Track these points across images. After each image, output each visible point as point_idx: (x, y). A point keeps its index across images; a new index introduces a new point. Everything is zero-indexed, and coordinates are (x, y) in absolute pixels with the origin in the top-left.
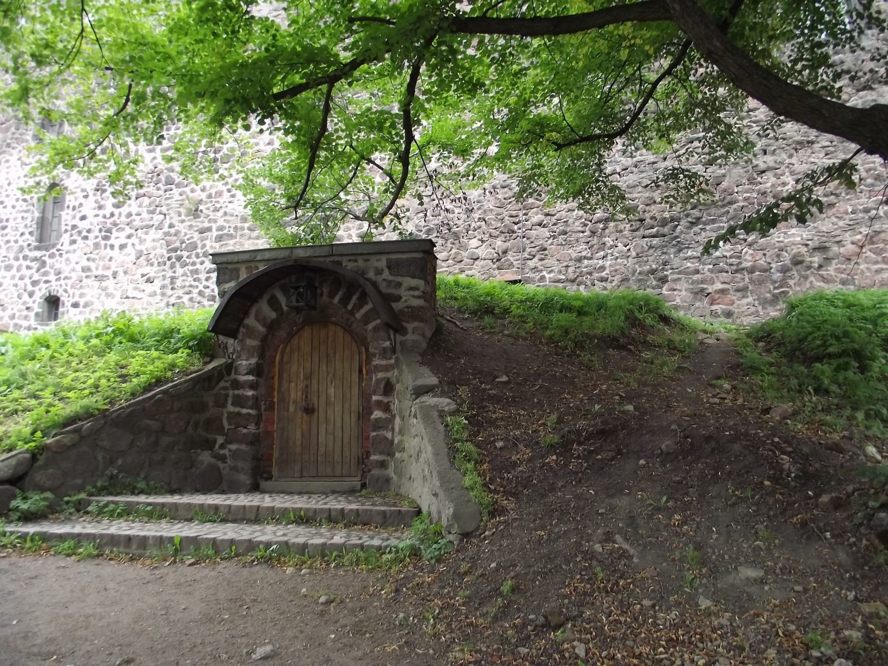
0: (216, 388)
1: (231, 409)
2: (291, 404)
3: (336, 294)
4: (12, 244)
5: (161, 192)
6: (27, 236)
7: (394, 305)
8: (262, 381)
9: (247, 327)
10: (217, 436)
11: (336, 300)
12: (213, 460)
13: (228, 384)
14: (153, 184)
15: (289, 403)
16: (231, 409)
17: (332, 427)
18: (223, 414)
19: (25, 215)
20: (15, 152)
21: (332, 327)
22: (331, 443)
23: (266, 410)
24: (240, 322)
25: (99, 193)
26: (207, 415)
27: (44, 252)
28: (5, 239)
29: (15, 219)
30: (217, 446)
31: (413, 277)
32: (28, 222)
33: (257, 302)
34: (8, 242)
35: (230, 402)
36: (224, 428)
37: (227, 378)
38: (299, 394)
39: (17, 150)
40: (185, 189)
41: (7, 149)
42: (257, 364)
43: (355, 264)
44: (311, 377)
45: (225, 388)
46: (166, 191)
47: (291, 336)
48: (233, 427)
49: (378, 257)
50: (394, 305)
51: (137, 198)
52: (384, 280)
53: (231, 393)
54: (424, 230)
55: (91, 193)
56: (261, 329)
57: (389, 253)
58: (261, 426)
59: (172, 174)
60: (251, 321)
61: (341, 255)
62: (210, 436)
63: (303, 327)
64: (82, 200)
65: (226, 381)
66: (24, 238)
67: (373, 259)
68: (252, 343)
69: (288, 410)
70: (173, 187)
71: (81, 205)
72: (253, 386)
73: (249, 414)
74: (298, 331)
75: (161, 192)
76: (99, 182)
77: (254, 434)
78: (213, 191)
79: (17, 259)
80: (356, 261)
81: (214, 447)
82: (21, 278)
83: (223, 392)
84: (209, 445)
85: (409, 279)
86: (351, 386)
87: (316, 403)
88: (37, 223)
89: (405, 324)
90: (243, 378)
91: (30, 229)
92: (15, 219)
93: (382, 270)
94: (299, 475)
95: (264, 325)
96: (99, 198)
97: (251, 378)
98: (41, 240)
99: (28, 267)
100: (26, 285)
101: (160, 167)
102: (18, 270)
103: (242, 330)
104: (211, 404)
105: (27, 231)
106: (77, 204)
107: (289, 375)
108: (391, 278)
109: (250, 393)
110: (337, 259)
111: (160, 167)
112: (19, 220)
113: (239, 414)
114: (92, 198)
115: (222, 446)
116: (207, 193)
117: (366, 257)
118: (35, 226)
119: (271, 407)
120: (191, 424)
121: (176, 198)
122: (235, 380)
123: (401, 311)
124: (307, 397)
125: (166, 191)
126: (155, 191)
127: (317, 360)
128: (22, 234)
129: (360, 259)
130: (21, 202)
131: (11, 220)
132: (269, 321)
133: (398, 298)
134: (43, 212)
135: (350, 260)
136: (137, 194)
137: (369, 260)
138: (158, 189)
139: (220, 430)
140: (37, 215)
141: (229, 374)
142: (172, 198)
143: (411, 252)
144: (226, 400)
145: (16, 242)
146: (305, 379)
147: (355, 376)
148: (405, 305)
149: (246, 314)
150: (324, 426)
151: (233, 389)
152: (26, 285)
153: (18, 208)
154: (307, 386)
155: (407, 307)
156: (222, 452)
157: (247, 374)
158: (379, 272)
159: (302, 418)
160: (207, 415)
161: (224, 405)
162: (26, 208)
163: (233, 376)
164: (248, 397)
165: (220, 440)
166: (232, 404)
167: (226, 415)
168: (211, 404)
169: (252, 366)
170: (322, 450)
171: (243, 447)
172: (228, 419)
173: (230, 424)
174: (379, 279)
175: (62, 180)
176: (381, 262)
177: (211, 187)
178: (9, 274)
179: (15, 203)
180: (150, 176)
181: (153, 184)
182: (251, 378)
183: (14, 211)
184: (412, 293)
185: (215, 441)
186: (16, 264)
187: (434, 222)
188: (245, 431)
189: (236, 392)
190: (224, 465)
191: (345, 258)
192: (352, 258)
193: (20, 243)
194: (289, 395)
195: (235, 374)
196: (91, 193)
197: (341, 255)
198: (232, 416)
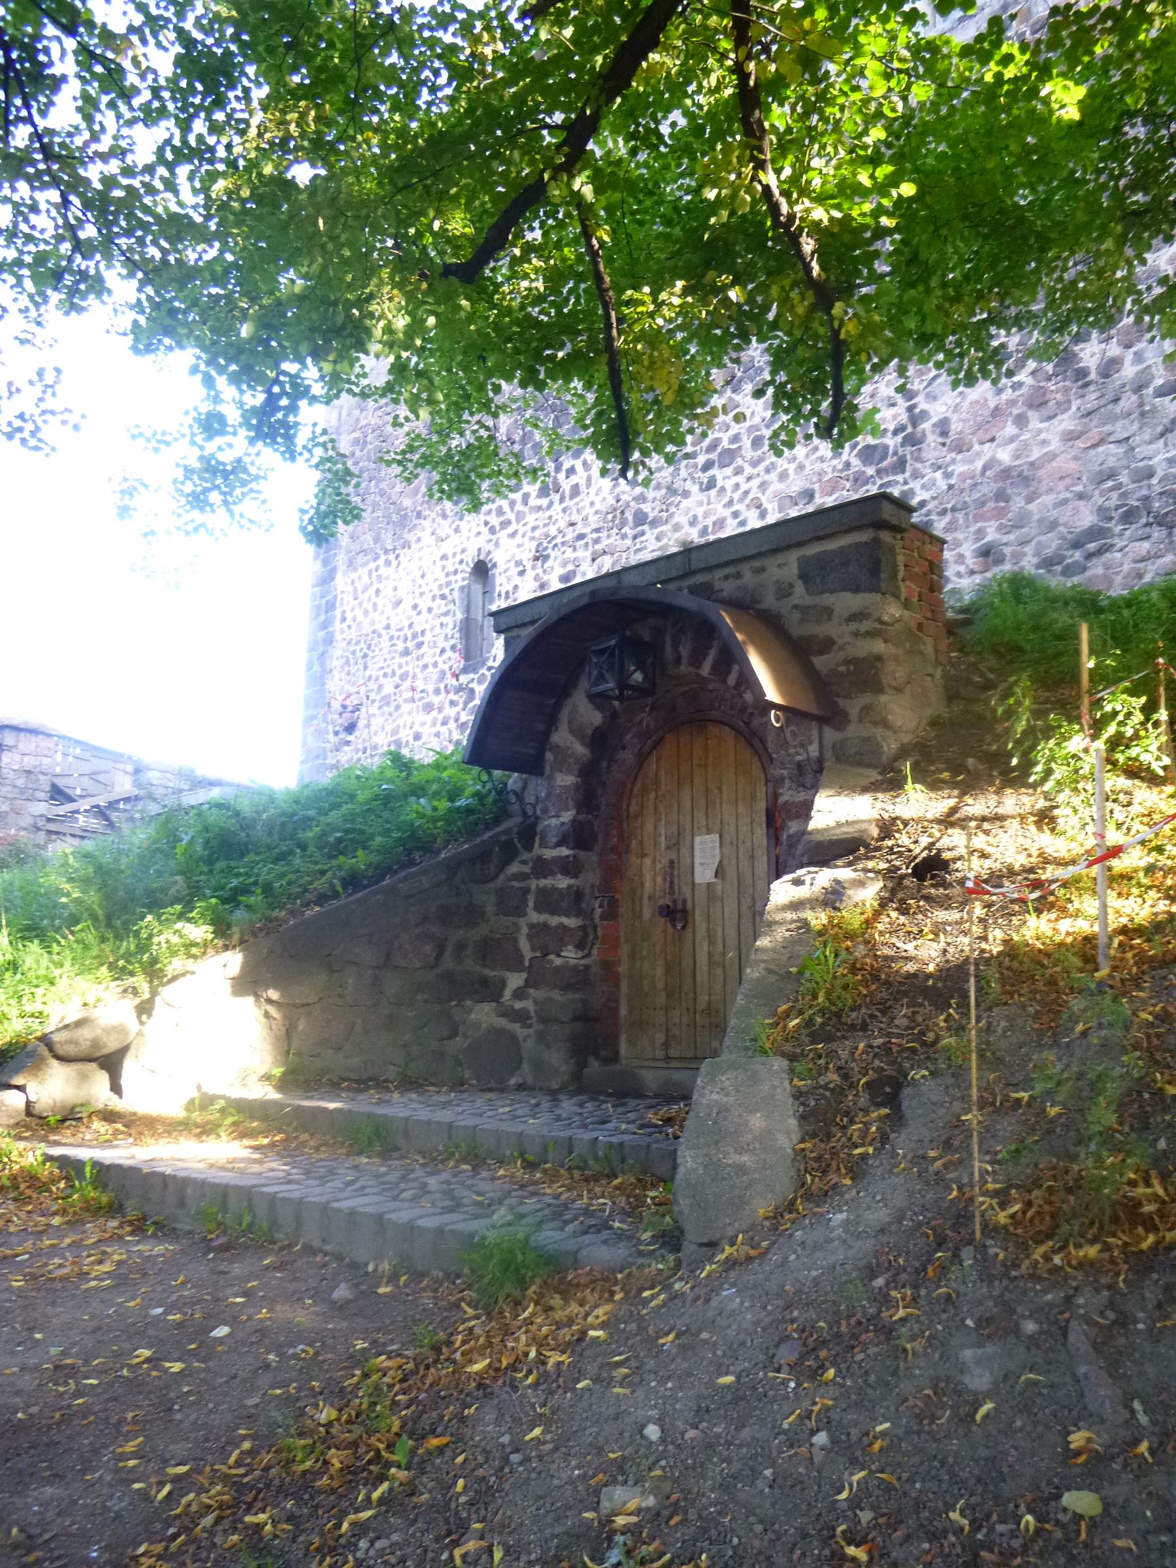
0: (502, 877)
1: (535, 917)
2: (646, 901)
3: (705, 655)
4: (431, 669)
5: (628, 542)
6: (449, 653)
7: (819, 662)
8: (591, 858)
9: (556, 749)
10: (508, 974)
11: (706, 669)
12: (502, 1022)
13: (527, 869)
14: (615, 531)
15: (641, 899)
16: (535, 917)
17: (720, 948)
18: (517, 928)
19: (444, 620)
20: (426, 523)
21: (714, 730)
22: (718, 986)
23: (603, 917)
24: (543, 740)
25: (539, 563)
26: (484, 929)
27: (472, 676)
28: (421, 663)
29: (432, 630)
30: (507, 994)
31: (857, 590)
32: (449, 630)
33: (570, 695)
34: (425, 666)
35: (531, 904)
36: (522, 957)
37: (526, 856)
38: (659, 879)
39: (429, 520)
40: (664, 528)
41: (417, 522)
42: (574, 821)
43: (738, 583)
44: (677, 844)
45: (524, 877)
46: (635, 537)
47: (642, 758)
48: (538, 954)
49: (780, 558)
50: (819, 662)
51: (593, 560)
52: (796, 607)
53: (533, 884)
54: (1116, 515)
55: (528, 565)
56: (580, 749)
57: (801, 544)
58: (595, 951)
59: (642, 506)
60: (562, 736)
61: (709, 569)
62: (490, 973)
63: (662, 738)
64: (517, 580)
65: (523, 862)
66: (445, 656)
67: (771, 563)
68: (565, 780)
69: (641, 916)
70: (646, 527)
71: (516, 587)
72: (570, 868)
73: (563, 927)
74: (655, 745)
75: (628, 542)
76: (540, 544)
77: (575, 967)
78: (709, 522)
79: (437, 692)
80: (738, 576)
81: (501, 995)
82: (444, 723)
83: (516, 884)
84: (490, 991)
85: (847, 595)
86: (752, 857)
87: (689, 897)
88: (460, 630)
89: (841, 702)
90: (549, 853)
91: (453, 642)
92: (432, 630)
93: (791, 586)
94: (660, 1054)
95: (582, 739)
96: (540, 571)
97: (564, 851)
98: (467, 658)
99: (453, 703)
100: (450, 733)
101: (624, 498)
102: (440, 710)
103: (549, 756)
104: (490, 909)
105: (448, 645)
106: (510, 588)
107: (641, 842)
108: (808, 600)
109: (563, 882)
110: (700, 579)
111: (624, 498)
112: (438, 630)
113: (545, 926)
114: (530, 574)
115: (519, 994)
116: (700, 527)
117: (756, 564)
118: (457, 635)
119: (611, 914)
120: (450, 949)
121: (651, 548)
122: (540, 858)
123: (833, 672)
124: (671, 887)
125: (635, 537)
126: (619, 542)
127: (688, 805)
128: (443, 651)
129: (746, 570)
130: (438, 601)
131: (427, 632)
132: (590, 731)
133: (827, 645)
134: (468, 609)
135: (726, 577)
136: (594, 553)
137: (763, 569)
138: (624, 536)
139: (515, 963)
140: (460, 616)
141: (529, 847)
142: (645, 548)
143: (847, 531)
144: (524, 901)
145: (435, 664)
146: (668, 848)
147: (761, 832)
148: (841, 655)
149: (552, 722)
150: (705, 945)
151: (538, 878)
152: (450, 733)
153: (435, 611)
154: (672, 862)
155: (847, 662)
156: (518, 1005)
157: (558, 844)
158: (784, 591)
159: (665, 931)
160: (484, 929)
161: (521, 913)
162: (444, 610)
163: (537, 850)
164: (560, 891)
165: (515, 980)
166: (536, 908)
167: (525, 930)
168: (490, 909)
169: (565, 828)
170: (703, 1000)
171: (557, 995)
172: (530, 937)
173: (533, 949)
174: (785, 606)
175: (489, 553)
176: (787, 567)
177: (706, 515)
178: (428, 719)
179: (430, 604)
180: (610, 517)
181: (615, 531)
182: (564, 851)
183: (430, 616)
184: (854, 626)
185: (503, 983)
186: (436, 700)
187: (1137, 495)
188: (558, 962)
189: (543, 882)
190: (526, 1031)
191: (718, 574)
192: (729, 570)
193: (441, 666)
194: (642, 884)
195: (541, 846)
196: (528, 565)
197: (709, 569)
198: (538, 931)
